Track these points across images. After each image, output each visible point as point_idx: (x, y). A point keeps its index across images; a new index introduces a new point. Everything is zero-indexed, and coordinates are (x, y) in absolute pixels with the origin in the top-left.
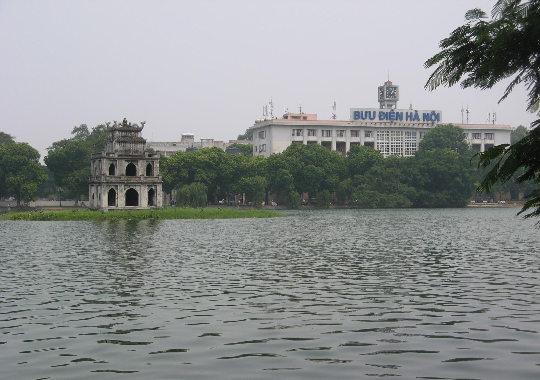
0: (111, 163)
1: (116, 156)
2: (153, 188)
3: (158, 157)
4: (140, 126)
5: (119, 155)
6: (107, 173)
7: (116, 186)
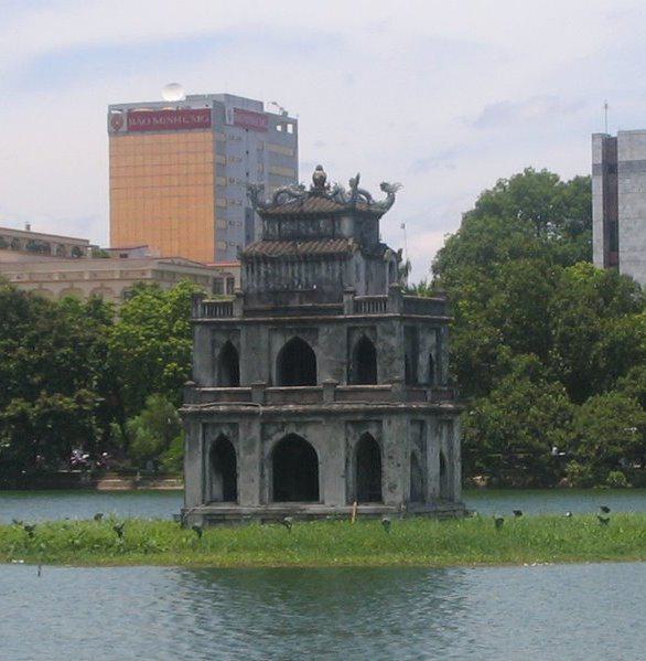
0: (223, 339)
1: (237, 315)
2: (373, 431)
3: (393, 311)
4: (379, 197)
5: (246, 313)
7: (234, 426)
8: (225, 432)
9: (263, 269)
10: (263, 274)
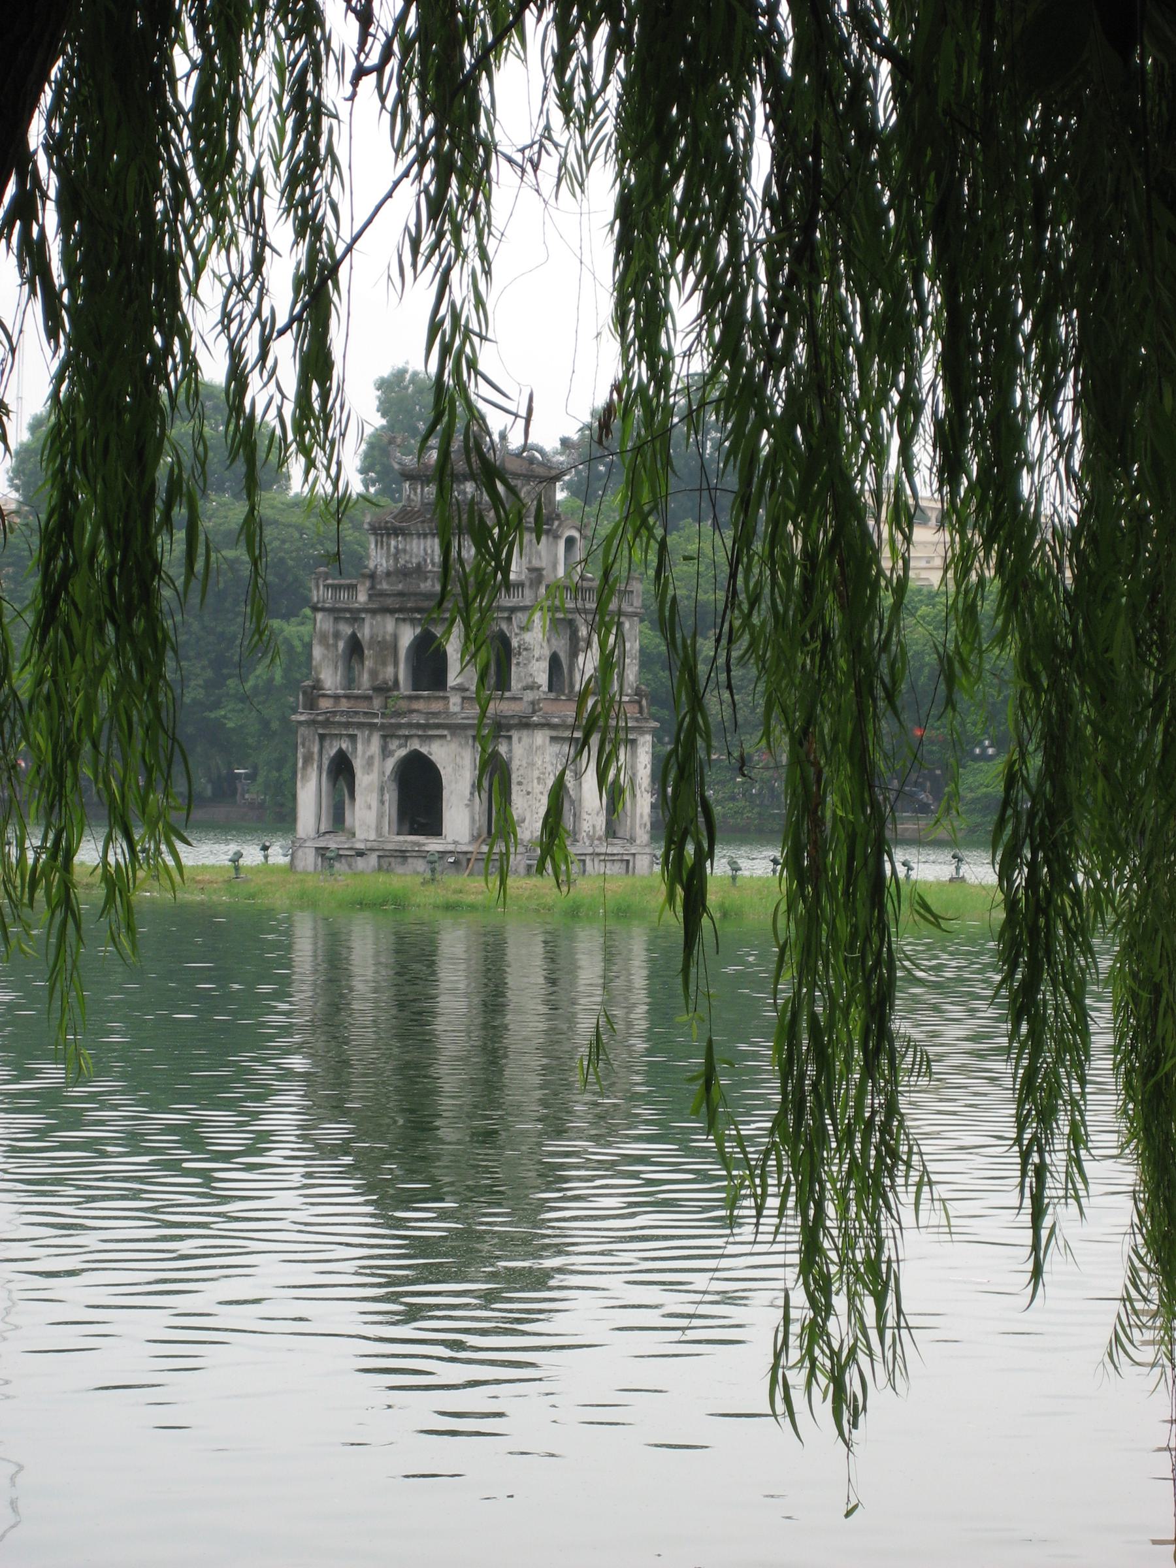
6: (543, 679)
7: (353, 738)
8: (344, 746)
9: (393, 543)
10: (392, 550)
